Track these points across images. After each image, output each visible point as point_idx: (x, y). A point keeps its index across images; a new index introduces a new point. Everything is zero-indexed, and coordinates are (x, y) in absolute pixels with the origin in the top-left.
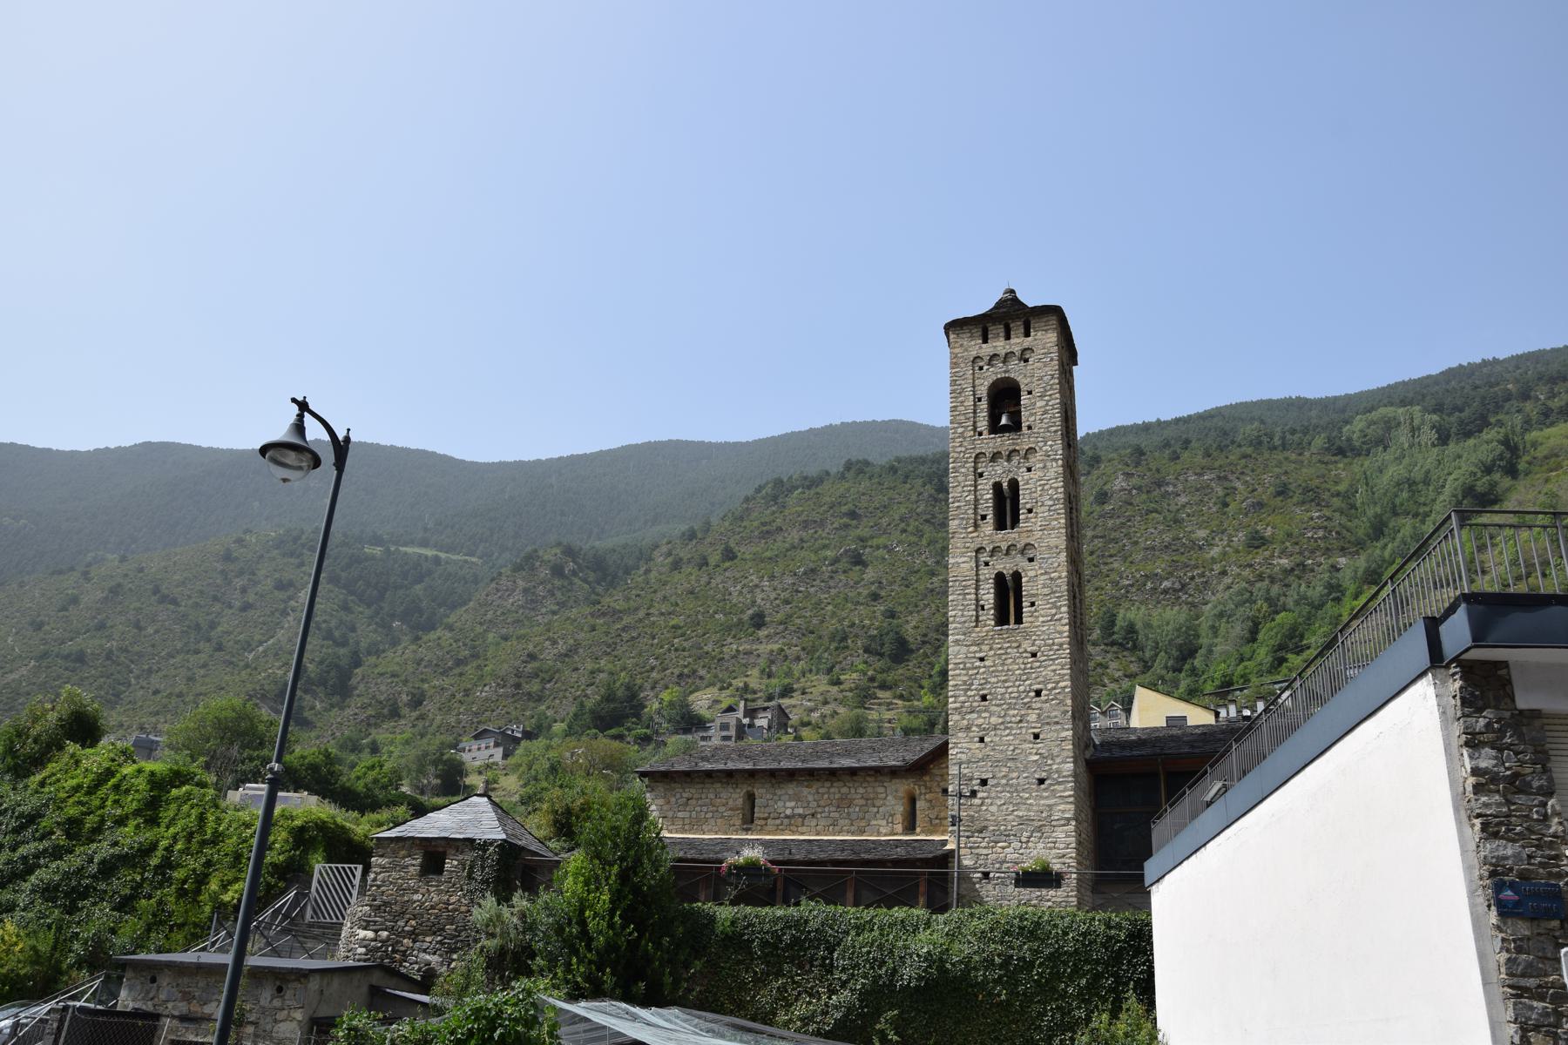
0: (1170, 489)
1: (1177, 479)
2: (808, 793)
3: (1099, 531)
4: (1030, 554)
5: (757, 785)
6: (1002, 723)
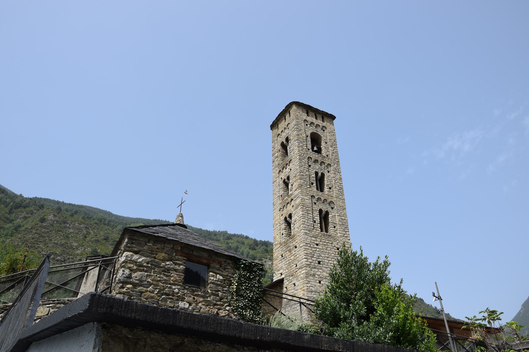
0: (68, 225)
1: (71, 223)
3: (38, 232)
4: (332, 206)
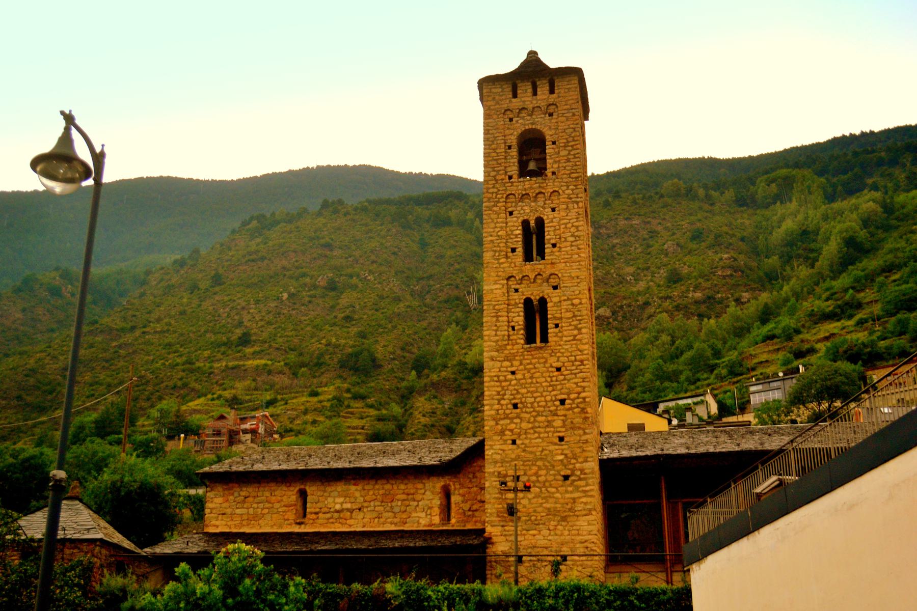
2: (355, 490)
4: (553, 281)
5: (308, 484)
6: (532, 428)
